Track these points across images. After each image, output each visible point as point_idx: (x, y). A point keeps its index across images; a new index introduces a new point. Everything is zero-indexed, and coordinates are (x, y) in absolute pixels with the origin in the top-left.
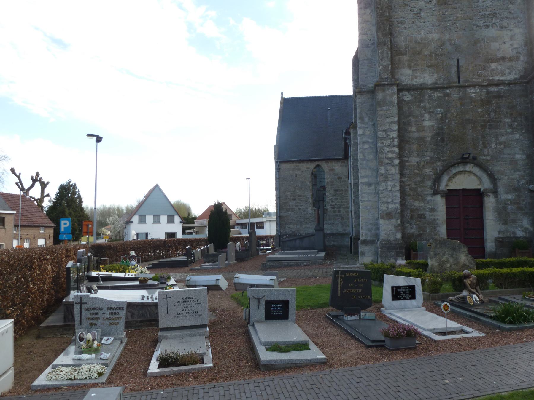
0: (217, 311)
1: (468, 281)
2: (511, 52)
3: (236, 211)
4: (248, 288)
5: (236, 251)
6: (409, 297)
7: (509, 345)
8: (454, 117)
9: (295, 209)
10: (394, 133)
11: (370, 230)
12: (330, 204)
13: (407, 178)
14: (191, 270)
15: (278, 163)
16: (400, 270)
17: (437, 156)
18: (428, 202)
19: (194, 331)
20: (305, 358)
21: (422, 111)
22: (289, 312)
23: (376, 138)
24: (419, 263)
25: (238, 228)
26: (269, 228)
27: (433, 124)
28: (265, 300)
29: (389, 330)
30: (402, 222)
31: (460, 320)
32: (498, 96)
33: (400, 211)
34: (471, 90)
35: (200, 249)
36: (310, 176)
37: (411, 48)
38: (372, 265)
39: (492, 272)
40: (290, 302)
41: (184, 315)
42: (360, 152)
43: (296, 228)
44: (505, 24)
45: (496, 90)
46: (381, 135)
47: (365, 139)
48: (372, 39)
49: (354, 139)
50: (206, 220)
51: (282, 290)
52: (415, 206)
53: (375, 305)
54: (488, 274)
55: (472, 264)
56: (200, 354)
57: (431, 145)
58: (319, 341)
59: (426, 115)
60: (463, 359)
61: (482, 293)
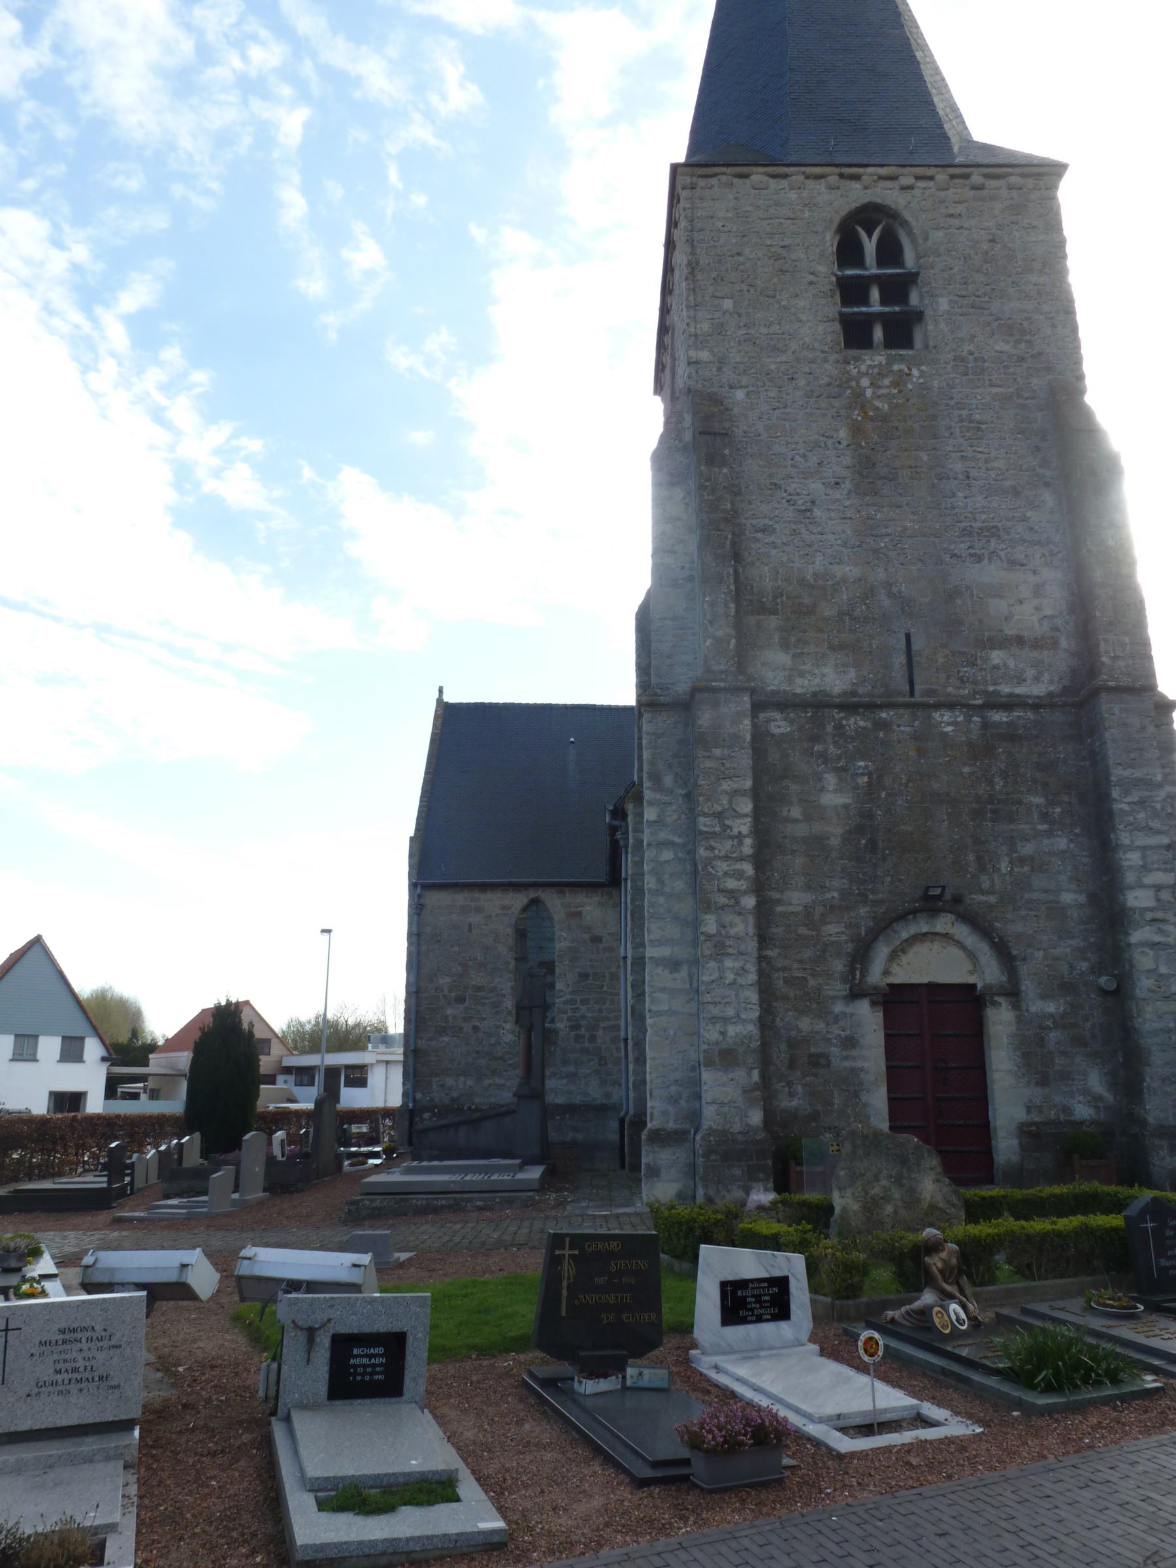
0: (181, 1369)
1: (935, 1262)
2: (1037, 624)
3: (285, 1028)
4: (280, 1293)
5: (270, 1160)
6: (771, 1314)
7: (1043, 1462)
8: (901, 785)
9: (461, 1028)
10: (743, 822)
11: (674, 1100)
12: (565, 1017)
13: (777, 950)
14: (118, 1221)
15: (419, 890)
16: (750, 1226)
17: (859, 889)
18: (837, 1019)
19: (91, 1444)
20: (438, 1531)
21: (818, 766)
22: (407, 1372)
23: (693, 835)
24: (804, 1204)
25: (286, 1082)
26: (383, 1085)
27: (848, 801)
28: (332, 1332)
29: (702, 1428)
30: (764, 1076)
31: (916, 1383)
32: (1011, 736)
33: (759, 1043)
34: (943, 715)
35: (153, 1151)
36: (509, 931)
37: (788, 598)
38: (673, 1211)
39: (1002, 1231)
40: (410, 1340)
41: (60, 1388)
42: (651, 872)
43: (461, 1086)
44: (1020, 557)
45: (1004, 719)
46: (708, 826)
47: (663, 835)
48: (687, 566)
49: (635, 831)
50: (186, 1053)
51: (389, 1299)
52: (799, 1031)
53: (670, 1342)
54: (994, 1239)
55: (954, 1205)
56: (96, 1530)
57: (841, 858)
58: (490, 1470)
59: (826, 776)
60: (913, 1513)
61: (977, 1296)
